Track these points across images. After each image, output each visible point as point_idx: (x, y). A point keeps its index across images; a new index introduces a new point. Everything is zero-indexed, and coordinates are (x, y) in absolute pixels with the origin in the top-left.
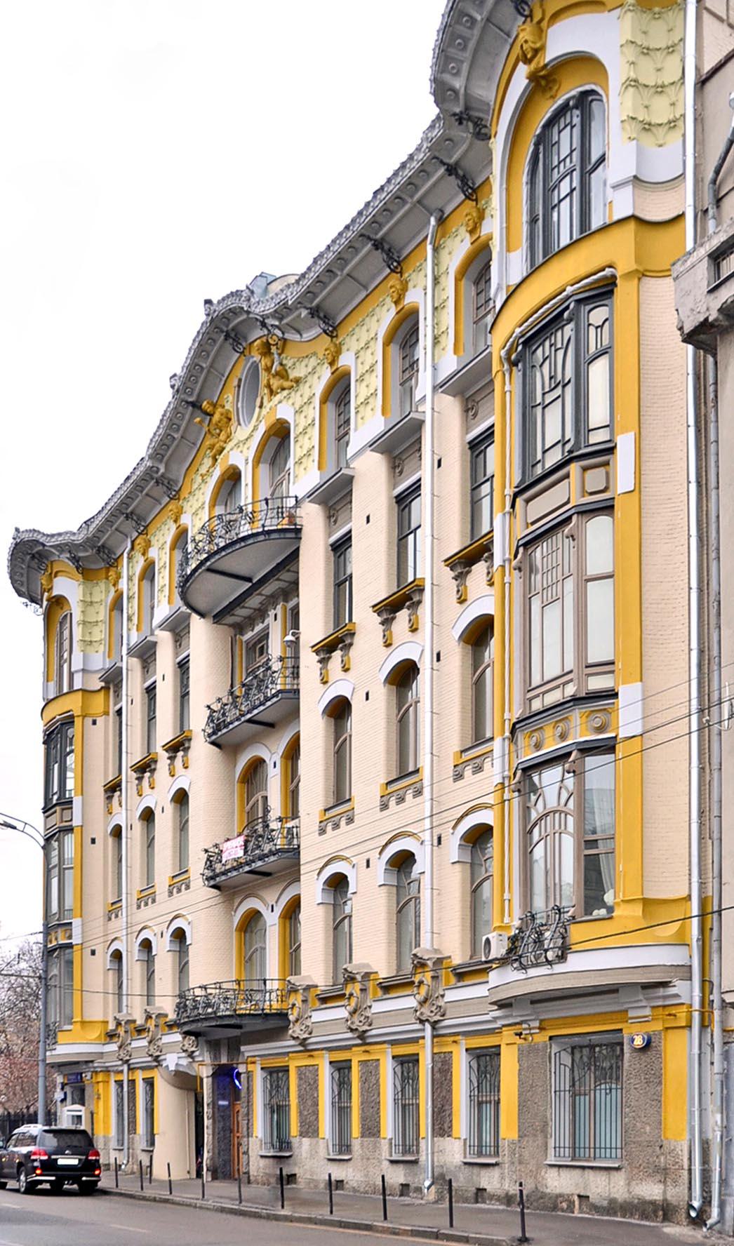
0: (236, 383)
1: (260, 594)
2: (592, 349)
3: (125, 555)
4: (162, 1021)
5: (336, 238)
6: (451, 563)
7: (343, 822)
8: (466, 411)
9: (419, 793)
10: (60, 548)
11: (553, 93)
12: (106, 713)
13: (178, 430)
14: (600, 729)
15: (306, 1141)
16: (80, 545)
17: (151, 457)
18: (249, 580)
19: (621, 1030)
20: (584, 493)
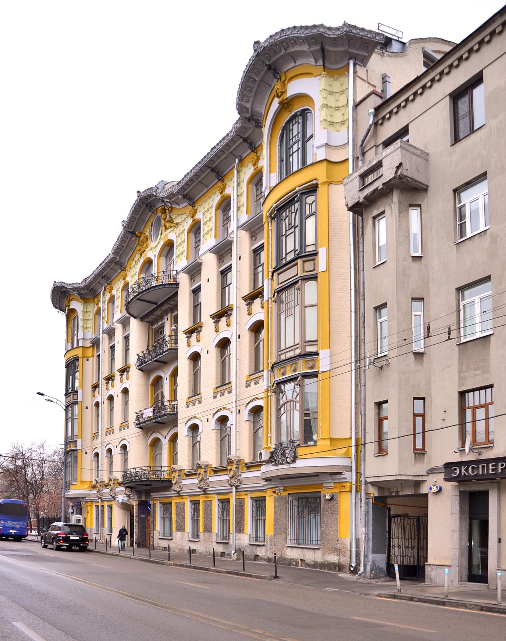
0: (150, 224)
2: (308, 213)
3: (102, 293)
4: (116, 482)
6: (245, 298)
9: (230, 392)
10: (73, 289)
11: (290, 109)
12: (93, 356)
14: (311, 368)
17: (113, 254)
18: (156, 304)
20: (304, 271)
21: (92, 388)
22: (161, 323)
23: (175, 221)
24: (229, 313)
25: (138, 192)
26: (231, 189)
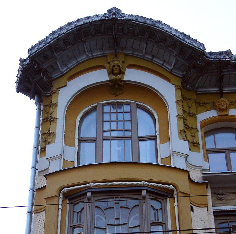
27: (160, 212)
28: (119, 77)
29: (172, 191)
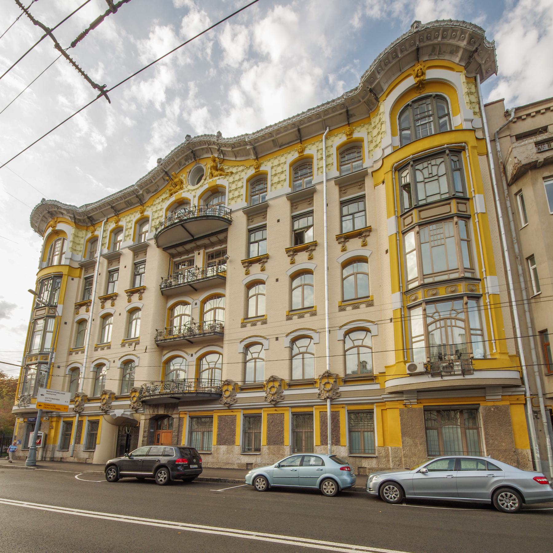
0: (189, 171)
1: (209, 239)
3: (103, 222)
4: (112, 396)
5: (260, 131)
6: (100, 298)
7: (106, 348)
8: (248, 220)
9: (83, 352)
10: (68, 211)
11: (421, 91)
12: (80, 277)
13: (154, 180)
14: (45, 360)
15: (223, 448)
16: (79, 213)
17: (138, 186)
18: (193, 236)
19: (479, 404)
21: (76, 306)
22: (223, 246)
23: (226, 171)
24: (89, 304)
25: (188, 136)
26: (99, 232)
27: (457, 163)
28: (422, 78)
29: (464, 147)
